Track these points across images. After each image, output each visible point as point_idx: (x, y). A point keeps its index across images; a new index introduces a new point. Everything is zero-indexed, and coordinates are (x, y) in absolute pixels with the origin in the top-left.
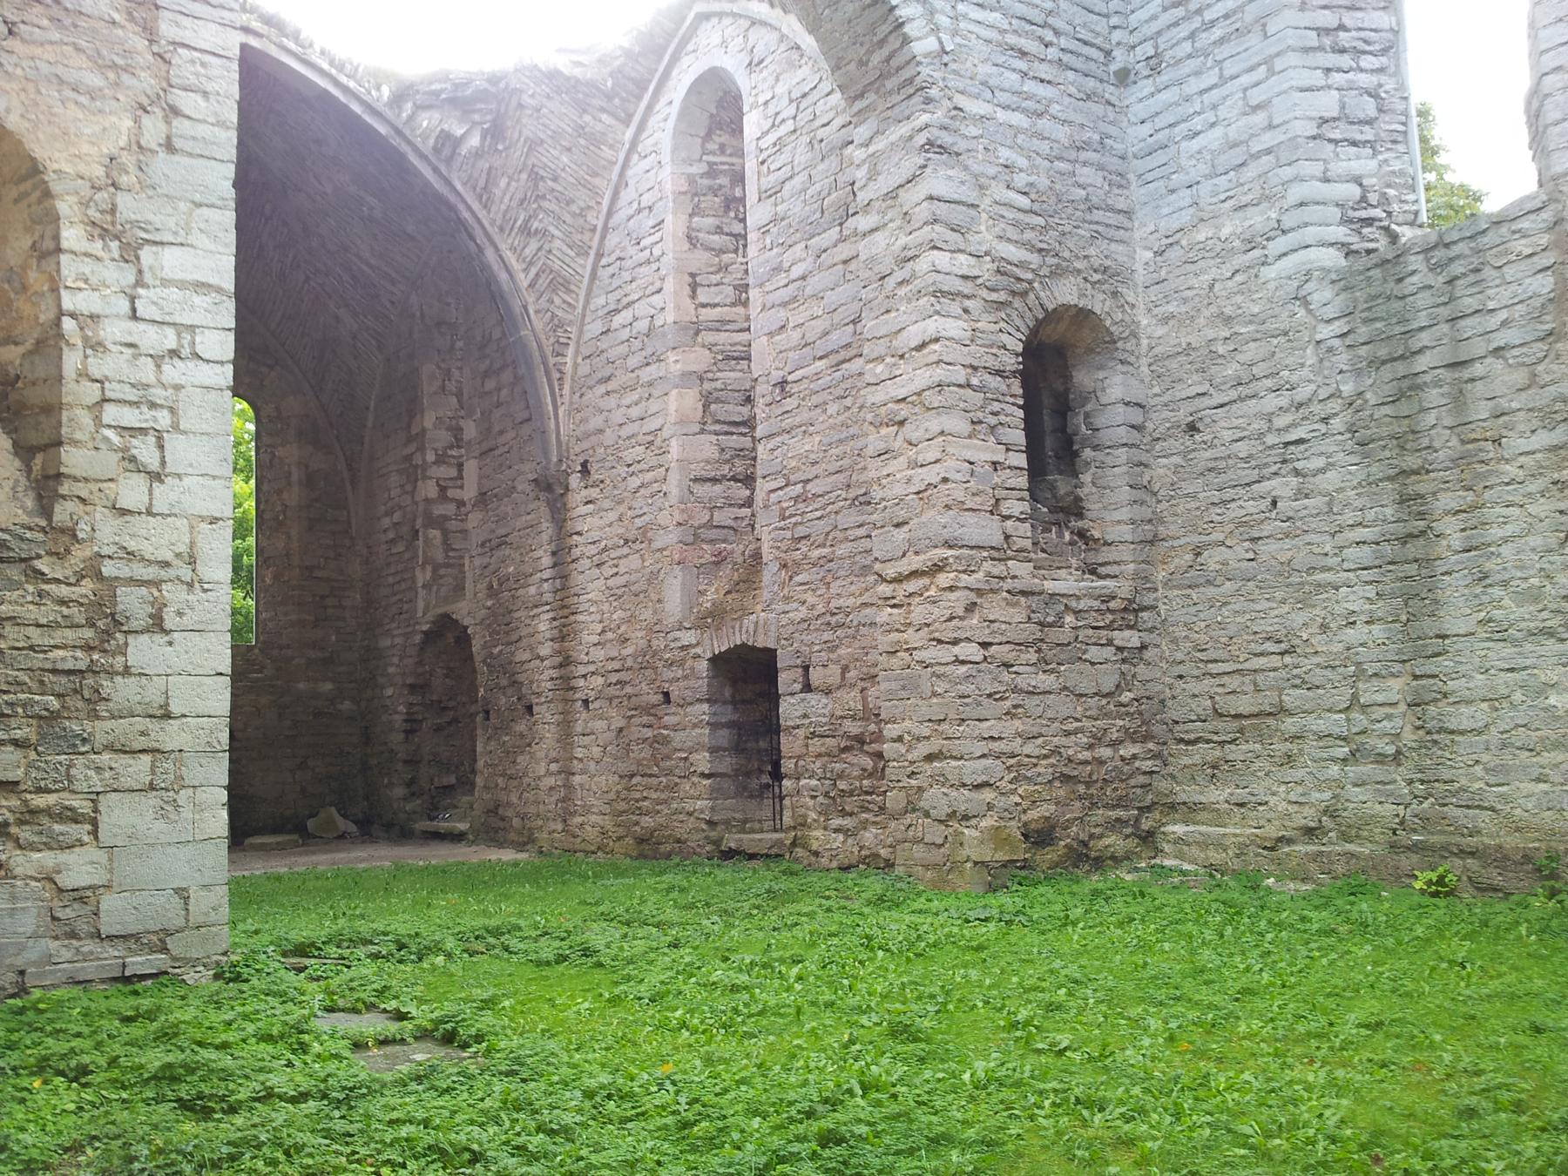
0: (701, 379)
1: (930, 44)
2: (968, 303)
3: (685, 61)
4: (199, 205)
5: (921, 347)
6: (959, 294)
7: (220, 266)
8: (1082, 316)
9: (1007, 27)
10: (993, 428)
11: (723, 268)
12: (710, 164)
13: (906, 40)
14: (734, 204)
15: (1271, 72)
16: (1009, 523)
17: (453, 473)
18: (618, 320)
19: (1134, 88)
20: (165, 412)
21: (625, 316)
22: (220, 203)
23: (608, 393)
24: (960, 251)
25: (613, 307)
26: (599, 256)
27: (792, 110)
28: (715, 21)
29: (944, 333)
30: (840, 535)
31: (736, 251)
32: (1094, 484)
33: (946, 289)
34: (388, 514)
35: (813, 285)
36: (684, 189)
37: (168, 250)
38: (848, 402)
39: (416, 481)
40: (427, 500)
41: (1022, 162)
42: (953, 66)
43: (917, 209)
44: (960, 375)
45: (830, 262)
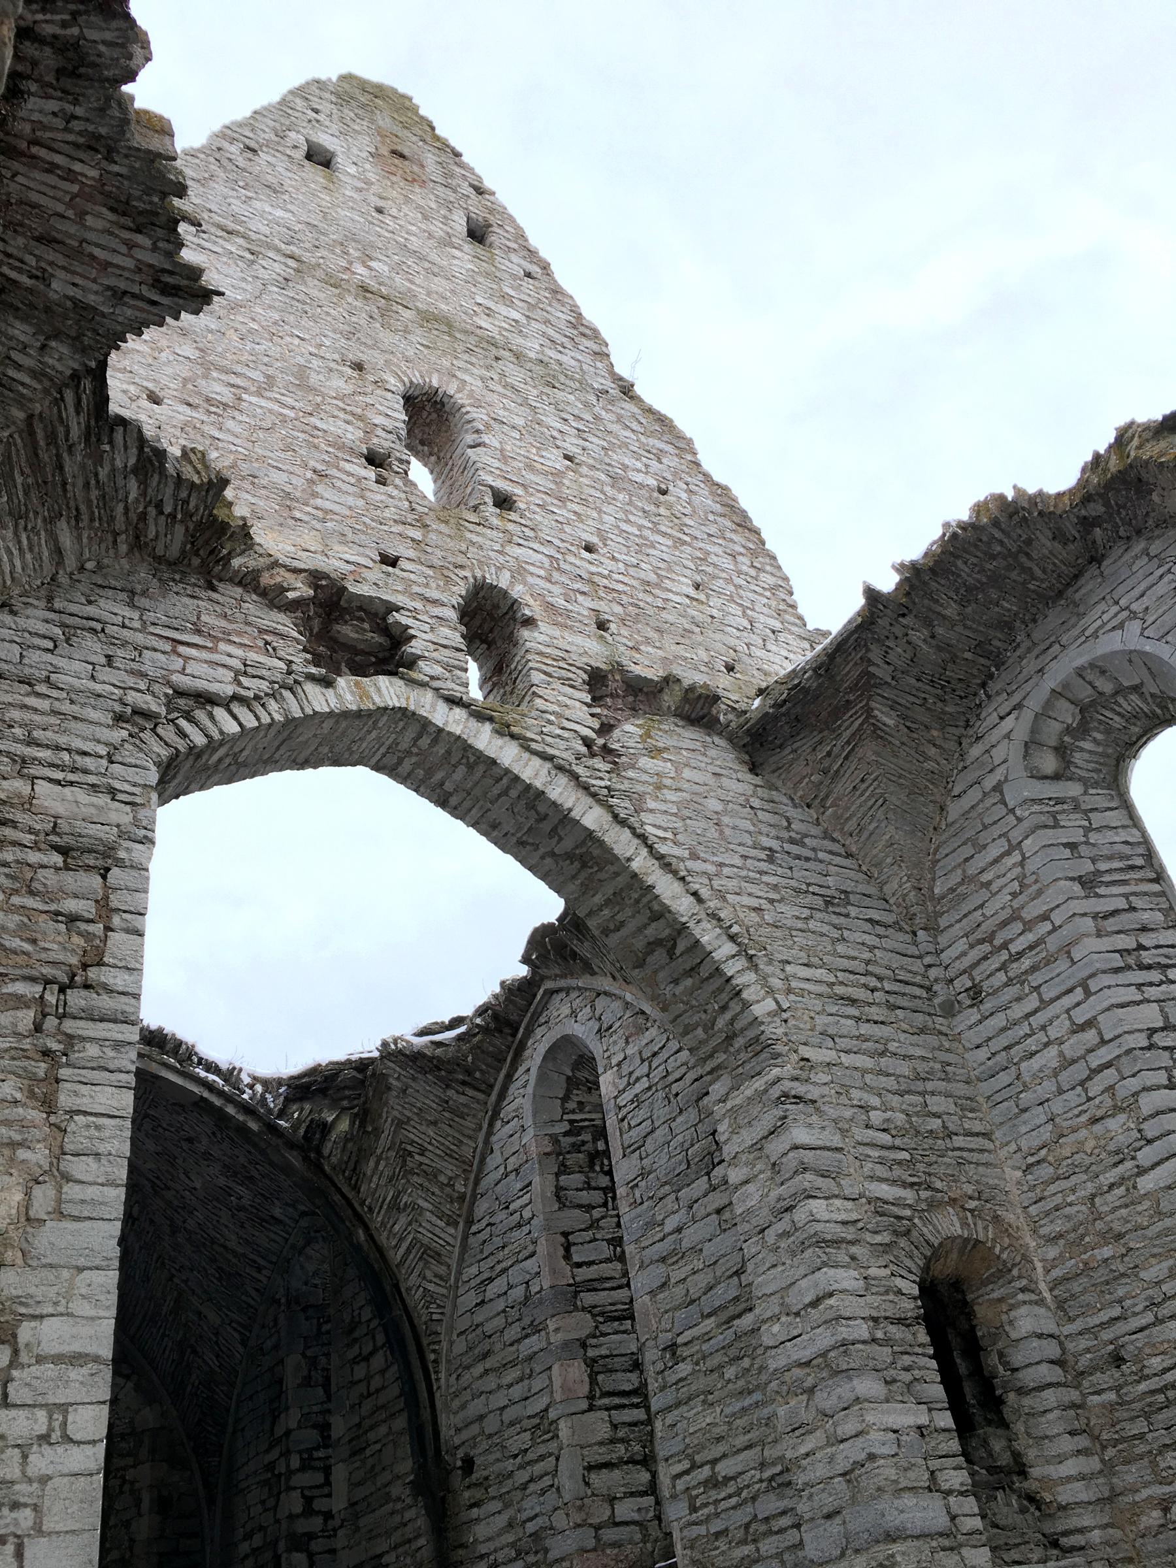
0: (584, 1345)
1: (770, 1005)
2: (854, 1250)
3: (539, 1032)
4: (80, 1270)
5: (815, 1304)
6: (843, 1241)
7: (98, 1334)
8: (971, 1246)
9: (833, 980)
10: (909, 1385)
11: (594, 1225)
12: (571, 1122)
13: (746, 1005)
14: (599, 1159)
15: (1088, 993)
16: (952, 1499)
17: (320, 1478)
18: (492, 1290)
19: (959, 1018)
20: (28, 1512)
21: (499, 1285)
22: (104, 1263)
23: (486, 1372)
24: (836, 1196)
25: (486, 1275)
26: (470, 1222)
27: (645, 1069)
28: (562, 995)
29: (836, 1286)
30: (763, 1528)
31: (605, 1205)
32: (1028, 1434)
33: (829, 1237)
34: (248, 1536)
35: (691, 1236)
36: (548, 1150)
37: (47, 1322)
38: (746, 1363)
39: (280, 1493)
40: (291, 1517)
41: (875, 1101)
42: (791, 1022)
43: (784, 1160)
44: (862, 1330)
45: (703, 1212)
